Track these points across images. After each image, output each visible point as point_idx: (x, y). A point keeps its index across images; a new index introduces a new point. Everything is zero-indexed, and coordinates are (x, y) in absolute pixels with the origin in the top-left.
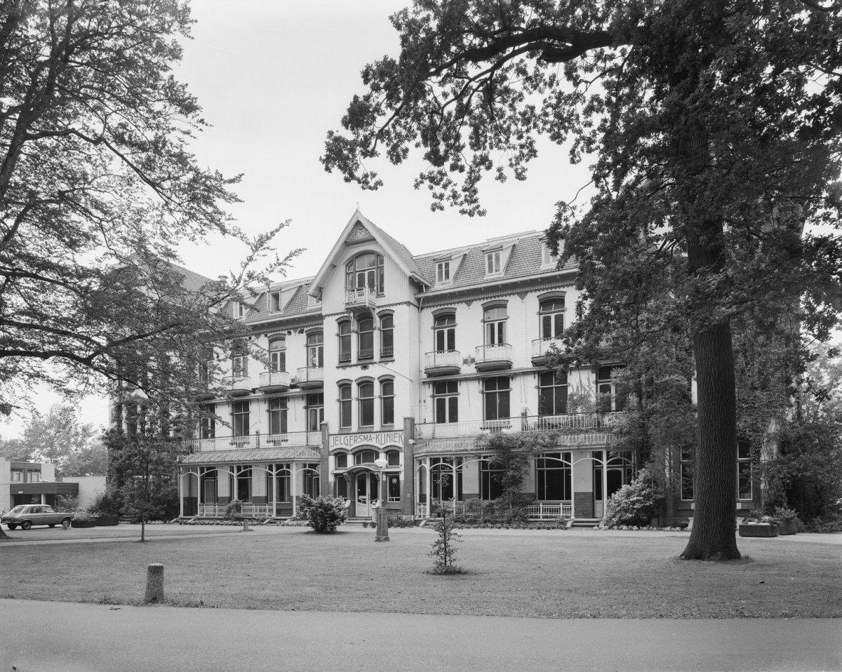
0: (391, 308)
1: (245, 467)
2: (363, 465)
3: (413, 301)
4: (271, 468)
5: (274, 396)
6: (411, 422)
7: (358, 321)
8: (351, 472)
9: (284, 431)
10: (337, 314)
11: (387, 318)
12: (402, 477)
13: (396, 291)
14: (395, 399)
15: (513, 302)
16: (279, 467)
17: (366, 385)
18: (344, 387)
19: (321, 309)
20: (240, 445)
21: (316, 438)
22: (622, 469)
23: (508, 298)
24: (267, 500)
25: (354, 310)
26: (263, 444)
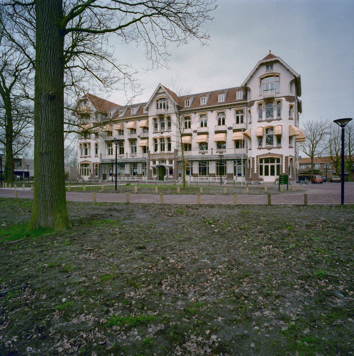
0: (280, 98)
2: (161, 164)
8: (157, 166)
11: (169, 118)
13: (172, 110)
15: (193, 115)
16: (134, 164)
17: (162, 139)
18: (155, 140)
20: (203, 153)
21: (146, 155)
23: (226, 110)
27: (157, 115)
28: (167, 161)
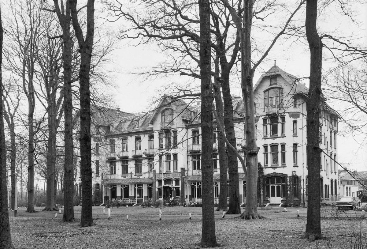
1: (127, 185)
2: (167, 185)
3: (184, 127)
4: (135, 186)
5: (123, 160)
6: (183, 169)
7: (270, 119)
9: (141, 172)
10: (263, 116)
11: (175, 132)
12: (180, 189)
14: (286, 153)
15: (129, 138)
16: (138, 185)
18: (265, 147)
19: (153, 128)
20: (125, 177)
22: (280, 185)
23: (141, 135)
24: (135, 197)
25: (269, 115)
26: (133, 176)
27: (267, 115)
28: (174, 182)
